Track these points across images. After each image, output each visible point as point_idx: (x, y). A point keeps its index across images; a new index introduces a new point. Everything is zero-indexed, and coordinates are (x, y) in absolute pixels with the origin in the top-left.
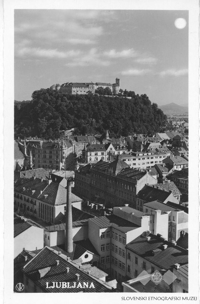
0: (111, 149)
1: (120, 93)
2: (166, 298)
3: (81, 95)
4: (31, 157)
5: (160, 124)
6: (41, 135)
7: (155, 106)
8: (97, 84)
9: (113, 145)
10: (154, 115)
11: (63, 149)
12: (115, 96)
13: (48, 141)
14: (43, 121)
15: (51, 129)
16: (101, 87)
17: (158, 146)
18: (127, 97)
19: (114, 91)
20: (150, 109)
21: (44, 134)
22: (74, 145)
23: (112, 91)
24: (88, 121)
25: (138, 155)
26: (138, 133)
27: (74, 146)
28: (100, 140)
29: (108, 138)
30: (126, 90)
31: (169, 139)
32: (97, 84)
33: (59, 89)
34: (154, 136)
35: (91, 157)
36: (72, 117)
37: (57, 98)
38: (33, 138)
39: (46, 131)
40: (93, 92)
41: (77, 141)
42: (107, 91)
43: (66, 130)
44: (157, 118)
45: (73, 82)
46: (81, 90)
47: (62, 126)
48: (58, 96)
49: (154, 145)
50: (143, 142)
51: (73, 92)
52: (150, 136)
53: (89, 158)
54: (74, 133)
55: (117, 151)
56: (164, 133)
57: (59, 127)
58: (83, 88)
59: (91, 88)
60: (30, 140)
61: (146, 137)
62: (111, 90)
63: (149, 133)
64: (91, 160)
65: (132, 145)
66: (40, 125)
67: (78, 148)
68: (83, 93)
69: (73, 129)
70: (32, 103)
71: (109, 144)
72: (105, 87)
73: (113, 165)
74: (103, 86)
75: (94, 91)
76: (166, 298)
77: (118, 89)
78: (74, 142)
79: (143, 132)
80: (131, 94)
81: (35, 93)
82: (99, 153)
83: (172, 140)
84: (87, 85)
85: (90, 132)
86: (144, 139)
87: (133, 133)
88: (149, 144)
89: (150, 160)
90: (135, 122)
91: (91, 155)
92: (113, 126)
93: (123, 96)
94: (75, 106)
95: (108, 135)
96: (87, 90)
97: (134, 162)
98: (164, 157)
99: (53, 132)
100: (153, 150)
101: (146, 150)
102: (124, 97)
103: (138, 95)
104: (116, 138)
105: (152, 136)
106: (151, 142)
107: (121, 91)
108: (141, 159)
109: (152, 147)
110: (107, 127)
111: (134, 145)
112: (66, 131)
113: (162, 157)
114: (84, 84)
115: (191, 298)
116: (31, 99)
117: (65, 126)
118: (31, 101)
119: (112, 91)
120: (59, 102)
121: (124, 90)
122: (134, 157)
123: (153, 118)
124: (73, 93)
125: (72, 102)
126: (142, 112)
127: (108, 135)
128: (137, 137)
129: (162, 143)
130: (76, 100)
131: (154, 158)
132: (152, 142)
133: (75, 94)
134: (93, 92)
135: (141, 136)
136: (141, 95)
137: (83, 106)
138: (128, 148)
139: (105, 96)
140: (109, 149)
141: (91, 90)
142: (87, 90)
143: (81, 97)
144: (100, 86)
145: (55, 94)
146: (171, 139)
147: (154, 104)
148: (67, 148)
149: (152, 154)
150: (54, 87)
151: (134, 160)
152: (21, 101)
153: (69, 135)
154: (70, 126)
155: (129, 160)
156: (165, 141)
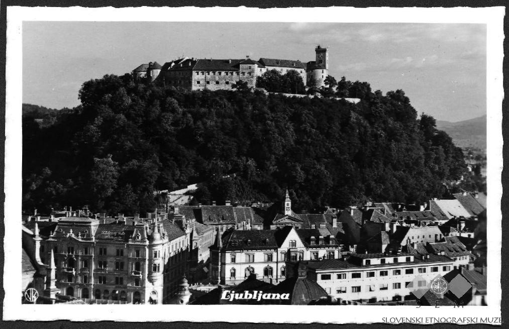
0: (294, 244)
1: (328, 86)
2: (454, 319)
3: (218, 93)
4: (53, 266)
5: (441, 175)
6: (101, 204)
7: (428, 121)
8: (262, 63)
9: (300, 232)
10: (426, 149)
11: (155, 243)
12: (312, 97)
13: (113, 220)
14: (107, 163)
15: (129, 186)
16: (274, 72)
17: (433, 237)
18: (346, 99)
19: (312, 81)
20: (412, 131)
21: (108, 200)
22: (188, 231)
23: (305, 82)
24: (237, 165)
25: (368, 262)
26: (379, 199)
27: (189, 236)
28: (267, 216)
29: (288, 212)
30: (344, 78)
31: (467, 215)
32: (262, 63)
33: (155, 77)
34: (422, 208)
35: (236, 267)
36: (191, 154)
37: (150, 102)
38: (77, 213)
39: (116, 192)
40: (252, 84)
41: (200, 220)
42: (292, 82)
43: (171, 189)
44: (434, 156)
45: (197, 57)
46: (217, 78)
47: (160, 178)
48: (153, 96)
49: (416, 235)
50: (387, 225)
51: (194, 83)
52: (410, 209)
53: (228, 269)
54: (197, 197)
55: (310, 249)
56: (453, 198)
57: (153, 180)
58: (223, 73)
59: (246, 75)
60: (63, 219)
61: (401, 210)
62: (301, 79)
63: (409, 200)
64: (233, 274)
65: (356, 233)
66: (98, 174)
67: (203, 239)
68: (223, 87)
69: (193, 187)
70: (80, 112)
71: (287, 230)
72: (283, 71)
73: (454, 218)
74: (278, 69)
75: (255, 81)
76: (454, 319)
77: (321, 75)
78: (191, 224)
79: (392, 194)
80: (360, 89)
81: (88, 86)
82: (260, 256)
83: (476, 219)
84: (235, 66)
85: (241, 196)
86: (394, 215)
87: (364, 198)
88: (407, 229)
89: (403, 278)
90: (370, 166)
91: (233, 260)
92: (307, 180)
93: (337, 94)
94: (199, 123)
95: (288, 203)
96: (235, 78)
97: (357, 282)
98: (445, 269)
99: (135, 198)
100: (416, 247)
101: (394, 249)
102: (338, 99)
103: (378, 93)
104: (312, 212)
105: (419, 209)
106: (413, 225)
107: (330, 80)
108: (377, 273)
109: (416, 237)
110: (286, 180)
111: (363, 231)
112: (172, 193)
113: (440, 268)
114: (227, 61)
115: (494, 319)
116: (78, 103)
117: (170, 177)
118: (76, 110)
119: (305, 82)
120: (156, 110)
121: (338, 80)
122: (357, 270)
123: (420, 157)
124: (195, 87)
125: (190, 112)
126: (390, 140)
127: (288, 203)
128: (371, 211)
129: (445, 229)
130: (204, 107)
131: (416, 270)
132: (418, 224)
133: (201, 88)
134: (252, 84)
135: (386, 207)
136: (389, 93)
137: (222, 122)
138: (343, 240)
139: (284, 94)
140: (285, 246)
141: (244, 78)
142: (235, 78)
143: (217, 99)
144: (271, 68)
145: (145, 90)
146: (473, 217)
147: (424, 118)
148: (166, 240)
149: (408, 259)
150: (144, 70)
151: (356, 276)
152: (59, 108)
153: (179, 202)
154: (184, 178)
155: (339, 277)
156: (454, 222)
